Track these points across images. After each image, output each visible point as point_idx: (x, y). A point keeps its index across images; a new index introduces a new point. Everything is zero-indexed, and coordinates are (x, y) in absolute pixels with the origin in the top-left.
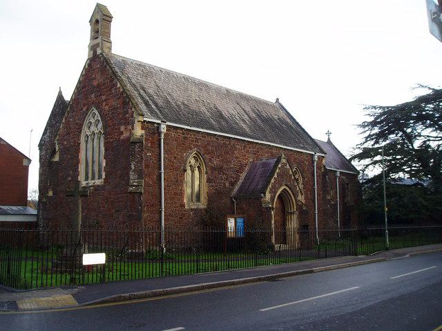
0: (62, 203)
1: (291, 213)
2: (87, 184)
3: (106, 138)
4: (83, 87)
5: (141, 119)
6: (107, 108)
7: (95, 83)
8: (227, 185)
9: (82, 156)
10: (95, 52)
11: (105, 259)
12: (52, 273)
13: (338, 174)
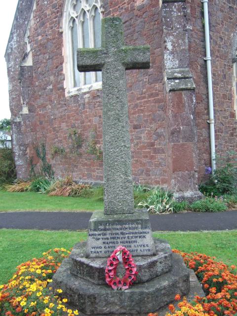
0: (41, 123)
11: (10, 116)
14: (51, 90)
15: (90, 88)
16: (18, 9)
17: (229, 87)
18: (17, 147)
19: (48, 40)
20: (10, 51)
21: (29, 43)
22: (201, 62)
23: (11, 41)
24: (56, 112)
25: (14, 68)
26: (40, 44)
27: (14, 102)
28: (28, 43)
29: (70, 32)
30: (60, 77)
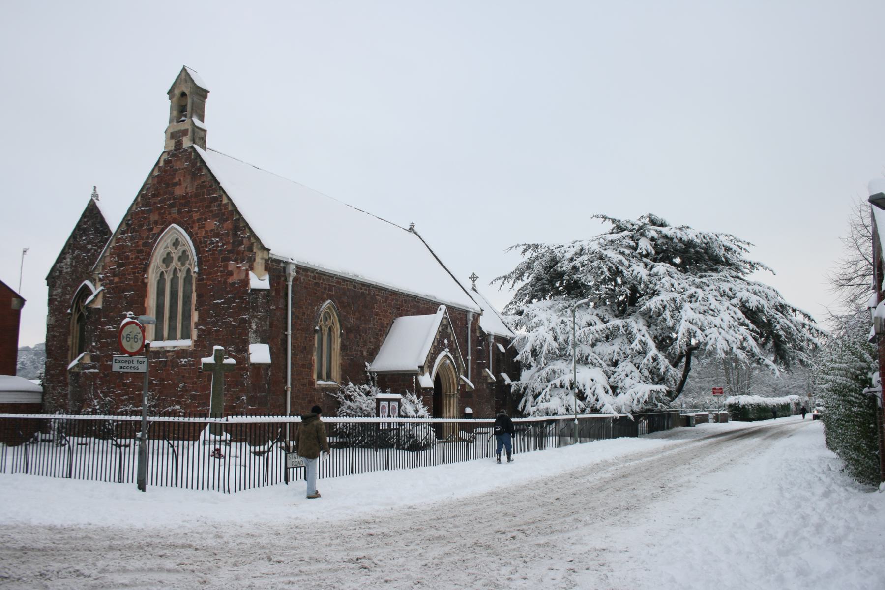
17: (309, 357)
18: (72, 402)
20: (57, 274)
22: (282, 336)
23: (61, 262)
25: (61, 297)
27: (54, 341)
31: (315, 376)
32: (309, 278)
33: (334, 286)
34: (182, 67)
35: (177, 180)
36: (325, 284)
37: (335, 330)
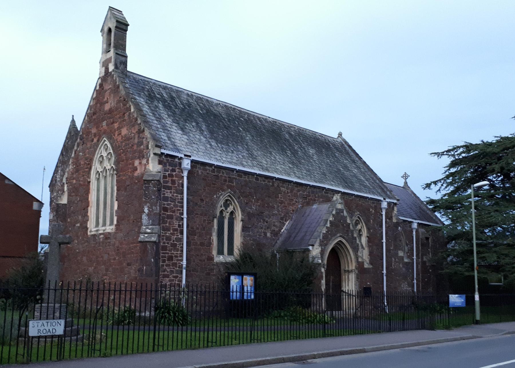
1: (349, 272)
2: (97, 231)
3: (118, 176)
4: (94, 114)
5: (158, 151)
6: (120, 138)
7: (107, 107)
8: (269, 235)
9: (92, 197)
10: (107, 69)
12: (169, 325)
13: (415, 226)
14: (79, 227)
15: (104, 230)
16: (64, 146)
19: (80, 185)
21: (67, 183)
24: (81, 246)
26: (74, 187)
28: (65, 183)
29: (96, 182)
30: (86, 217)
31: (214, 252)
32: (208, 172)
33: (236, 179)
34: (108, 8)
35: (106, 99)
36: (226, 177)
37: (237, 215)
